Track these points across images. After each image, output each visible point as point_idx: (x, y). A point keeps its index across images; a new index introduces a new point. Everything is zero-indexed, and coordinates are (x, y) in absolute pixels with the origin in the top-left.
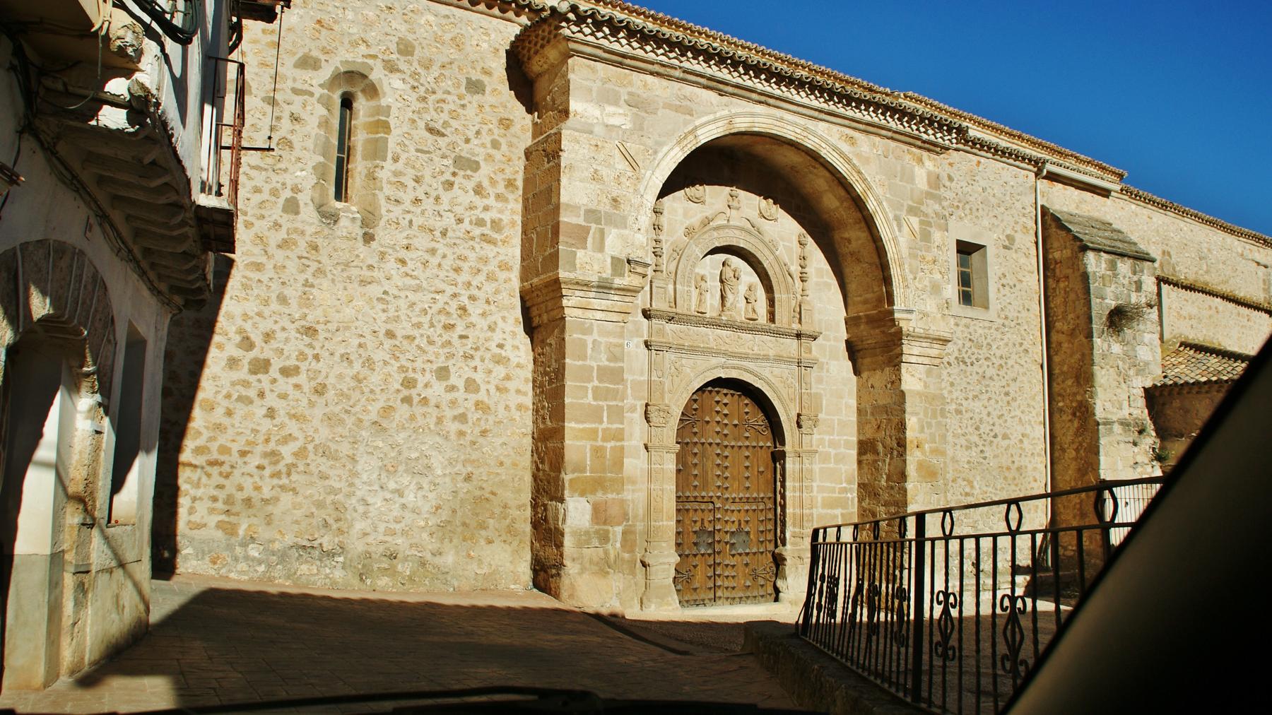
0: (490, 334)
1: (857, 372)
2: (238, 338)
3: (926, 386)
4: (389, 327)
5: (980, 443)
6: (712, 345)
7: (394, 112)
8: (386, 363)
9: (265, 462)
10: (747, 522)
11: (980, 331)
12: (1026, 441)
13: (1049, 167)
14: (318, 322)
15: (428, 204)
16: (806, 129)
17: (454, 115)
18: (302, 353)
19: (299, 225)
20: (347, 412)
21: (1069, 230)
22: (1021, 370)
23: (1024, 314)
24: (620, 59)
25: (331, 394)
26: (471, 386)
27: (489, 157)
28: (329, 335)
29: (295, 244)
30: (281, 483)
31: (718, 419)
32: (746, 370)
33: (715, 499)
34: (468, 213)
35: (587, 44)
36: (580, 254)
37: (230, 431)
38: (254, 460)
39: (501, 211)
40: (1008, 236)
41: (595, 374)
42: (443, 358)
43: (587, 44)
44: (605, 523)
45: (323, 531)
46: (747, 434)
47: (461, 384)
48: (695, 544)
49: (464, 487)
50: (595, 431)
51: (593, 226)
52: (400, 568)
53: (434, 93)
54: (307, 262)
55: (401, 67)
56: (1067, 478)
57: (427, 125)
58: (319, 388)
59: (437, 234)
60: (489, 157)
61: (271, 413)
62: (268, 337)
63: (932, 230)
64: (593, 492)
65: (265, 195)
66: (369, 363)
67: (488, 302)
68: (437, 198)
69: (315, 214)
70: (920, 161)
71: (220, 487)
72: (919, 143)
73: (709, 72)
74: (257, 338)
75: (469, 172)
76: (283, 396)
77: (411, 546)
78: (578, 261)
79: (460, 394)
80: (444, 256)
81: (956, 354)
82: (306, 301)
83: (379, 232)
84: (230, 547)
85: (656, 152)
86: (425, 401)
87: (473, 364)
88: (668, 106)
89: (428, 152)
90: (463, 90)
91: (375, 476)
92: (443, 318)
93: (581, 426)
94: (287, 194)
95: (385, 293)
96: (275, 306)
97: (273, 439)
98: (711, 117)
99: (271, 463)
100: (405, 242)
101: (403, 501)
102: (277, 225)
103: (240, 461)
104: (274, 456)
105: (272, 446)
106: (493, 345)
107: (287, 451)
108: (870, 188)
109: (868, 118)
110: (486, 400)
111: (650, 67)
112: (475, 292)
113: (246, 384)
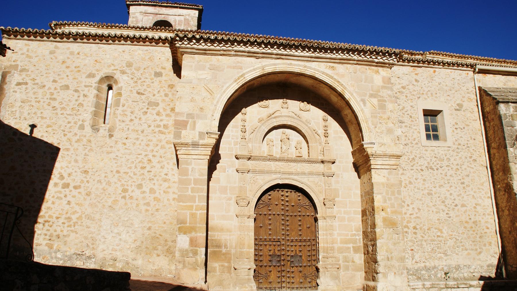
0: (161, 170)
1: (359, 177)
2: (59, 176)
3: (388, 179)
4: (118, 169)
5: (446, 209)
6: (273, 169)
7: (124, 88)
8: (115, 183)
9: (65, 221)
10: (300, 251)
11: (442, 152)
12: (478, 208)
13: (479, 67)
14: (89, 169)
15: (136, 121)
16: (305, 67)
17: (149, 86)
18: (82, 180)
19: (84, 134)
20: (99, 202)
21: (491, 95)
22: (472, 170)
23: (472, 141)
24: (204, 52)
25: (93, 196)
26: (152, 191)
27: (164, 100)
28: (93, 173)
29: (82, 140)
30: (71, 229)
31: (283, 203)
32: (293, 179)
33: (281, 240)
34: (153, 123)
35: (187, 48)
36: (183, 132)
37: (53, 210)
38: (61, 220)
39: (168, 121)
40: (458, 105)
41: (192, 182)
42: (140, 180)
43: (187, 48)
44: (196, 246)
45: (86, 248)
46: (299, 210)
47: (148, 191)
48: (270, 261)
49: (148, 232)
50: (192, 206)
51: (190, 120)
52: (117, 265)
53: (140, 79)
54: (86, 147)
55: (127, 72)
56: (507, 226)
57: (137, 91)
58: (88, 193)
59: (140, 132)
60: (164, 100)
61: (69, 203)
62: (69, 175)
63: (386, 104)
64: (190, 232)
65: (72, 124)
66: (109, 183)
67: (161, 157)
68: (140, 119)
69: (91, 129)
70: (378, 72)
71: (48, 230)
72: (375, 64)
73: (247, 49)
74: (65, 175)
75: (154, 107)
76: (74, 197)
77: (123, 256)
78: (182, 135)
79: (147, 195)
80: (142, 140)
81: (426, 165)
82: (85, 160)
83: (115, 134)
84: (50, 253)
85: (223, 87)
86: (131, 198)
87: (153, 182)
88: (229, 67)
89: (137, 102)
90: (153, 76)
91: (109, 227)
92: (141, 165)
93: (185, 204)
94: (81, 123)
95: (117, 156)
96: (73, 163)
97: (69, 213)
98: (252, 68)
99: (68, 222)
100: (126, 136)
101: (120, 237)
102: (76, 134)
103: (56, 221)
104: (69, 219)
105: (68, 215)
106: (163, 174)
107: (74, 217)
108: (345, 88)
109: (339, 57)
110: (159, 197)
111: (219, 52)
112: (154, 153)
113: (60, 192)
